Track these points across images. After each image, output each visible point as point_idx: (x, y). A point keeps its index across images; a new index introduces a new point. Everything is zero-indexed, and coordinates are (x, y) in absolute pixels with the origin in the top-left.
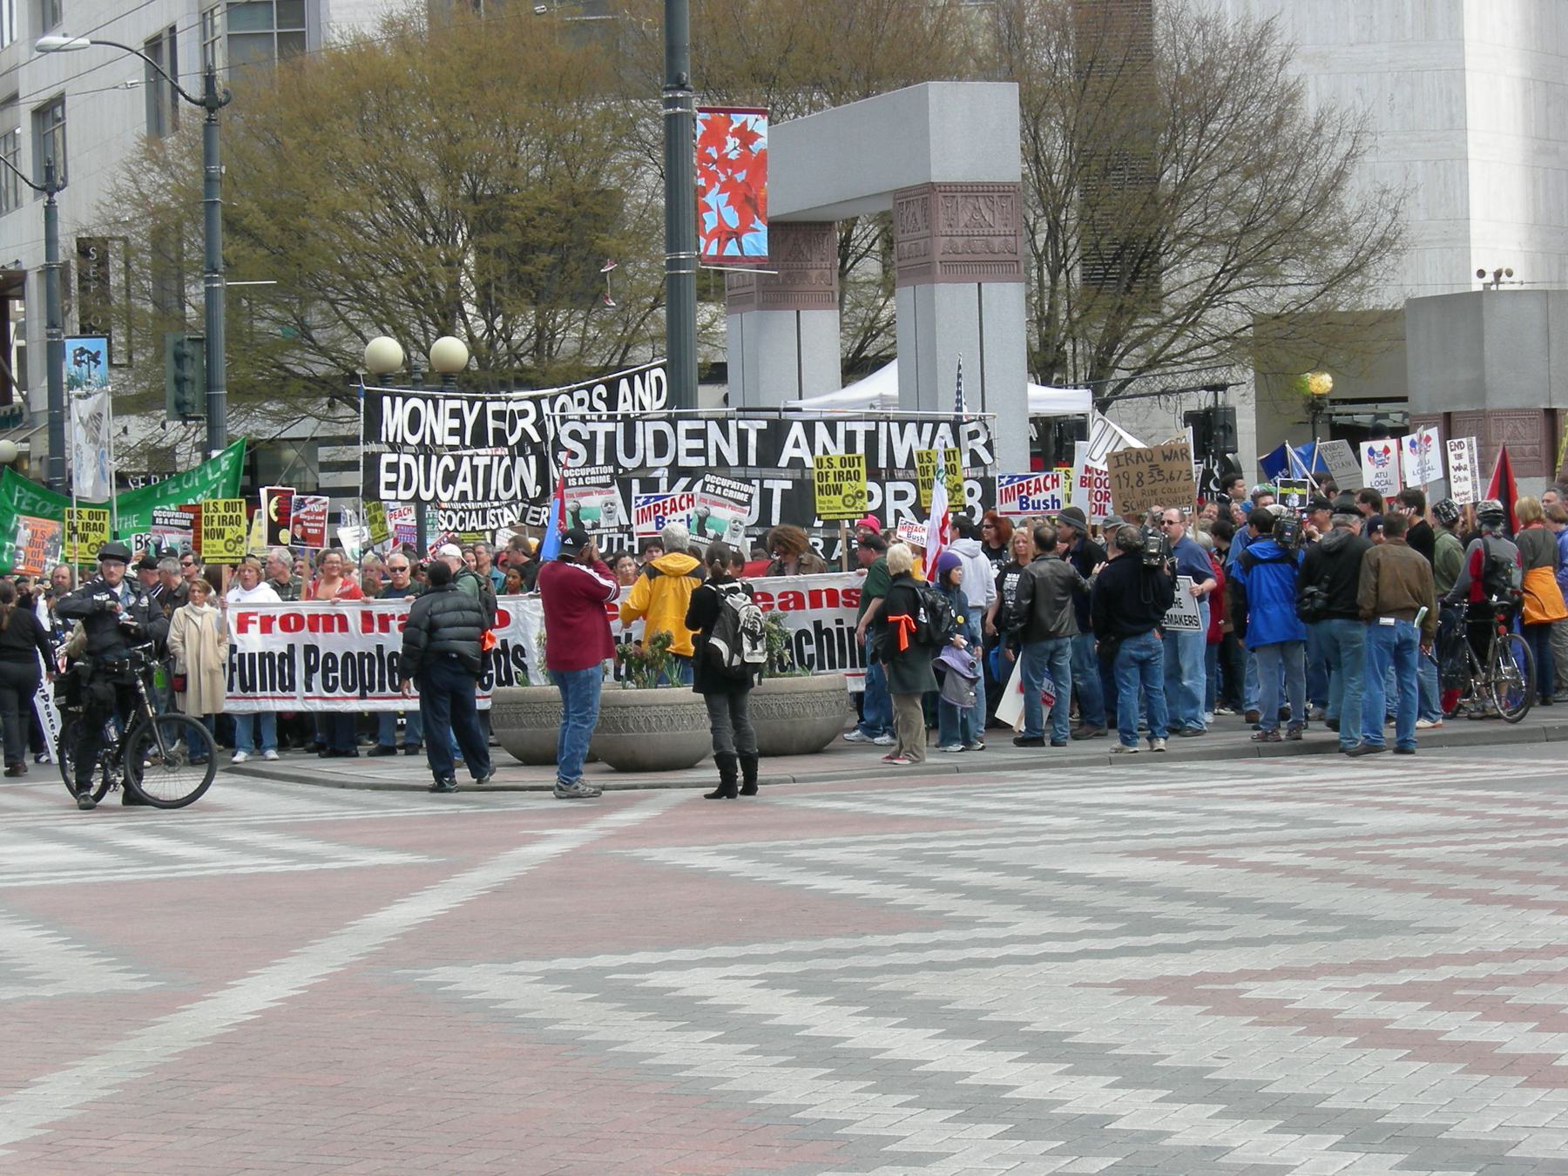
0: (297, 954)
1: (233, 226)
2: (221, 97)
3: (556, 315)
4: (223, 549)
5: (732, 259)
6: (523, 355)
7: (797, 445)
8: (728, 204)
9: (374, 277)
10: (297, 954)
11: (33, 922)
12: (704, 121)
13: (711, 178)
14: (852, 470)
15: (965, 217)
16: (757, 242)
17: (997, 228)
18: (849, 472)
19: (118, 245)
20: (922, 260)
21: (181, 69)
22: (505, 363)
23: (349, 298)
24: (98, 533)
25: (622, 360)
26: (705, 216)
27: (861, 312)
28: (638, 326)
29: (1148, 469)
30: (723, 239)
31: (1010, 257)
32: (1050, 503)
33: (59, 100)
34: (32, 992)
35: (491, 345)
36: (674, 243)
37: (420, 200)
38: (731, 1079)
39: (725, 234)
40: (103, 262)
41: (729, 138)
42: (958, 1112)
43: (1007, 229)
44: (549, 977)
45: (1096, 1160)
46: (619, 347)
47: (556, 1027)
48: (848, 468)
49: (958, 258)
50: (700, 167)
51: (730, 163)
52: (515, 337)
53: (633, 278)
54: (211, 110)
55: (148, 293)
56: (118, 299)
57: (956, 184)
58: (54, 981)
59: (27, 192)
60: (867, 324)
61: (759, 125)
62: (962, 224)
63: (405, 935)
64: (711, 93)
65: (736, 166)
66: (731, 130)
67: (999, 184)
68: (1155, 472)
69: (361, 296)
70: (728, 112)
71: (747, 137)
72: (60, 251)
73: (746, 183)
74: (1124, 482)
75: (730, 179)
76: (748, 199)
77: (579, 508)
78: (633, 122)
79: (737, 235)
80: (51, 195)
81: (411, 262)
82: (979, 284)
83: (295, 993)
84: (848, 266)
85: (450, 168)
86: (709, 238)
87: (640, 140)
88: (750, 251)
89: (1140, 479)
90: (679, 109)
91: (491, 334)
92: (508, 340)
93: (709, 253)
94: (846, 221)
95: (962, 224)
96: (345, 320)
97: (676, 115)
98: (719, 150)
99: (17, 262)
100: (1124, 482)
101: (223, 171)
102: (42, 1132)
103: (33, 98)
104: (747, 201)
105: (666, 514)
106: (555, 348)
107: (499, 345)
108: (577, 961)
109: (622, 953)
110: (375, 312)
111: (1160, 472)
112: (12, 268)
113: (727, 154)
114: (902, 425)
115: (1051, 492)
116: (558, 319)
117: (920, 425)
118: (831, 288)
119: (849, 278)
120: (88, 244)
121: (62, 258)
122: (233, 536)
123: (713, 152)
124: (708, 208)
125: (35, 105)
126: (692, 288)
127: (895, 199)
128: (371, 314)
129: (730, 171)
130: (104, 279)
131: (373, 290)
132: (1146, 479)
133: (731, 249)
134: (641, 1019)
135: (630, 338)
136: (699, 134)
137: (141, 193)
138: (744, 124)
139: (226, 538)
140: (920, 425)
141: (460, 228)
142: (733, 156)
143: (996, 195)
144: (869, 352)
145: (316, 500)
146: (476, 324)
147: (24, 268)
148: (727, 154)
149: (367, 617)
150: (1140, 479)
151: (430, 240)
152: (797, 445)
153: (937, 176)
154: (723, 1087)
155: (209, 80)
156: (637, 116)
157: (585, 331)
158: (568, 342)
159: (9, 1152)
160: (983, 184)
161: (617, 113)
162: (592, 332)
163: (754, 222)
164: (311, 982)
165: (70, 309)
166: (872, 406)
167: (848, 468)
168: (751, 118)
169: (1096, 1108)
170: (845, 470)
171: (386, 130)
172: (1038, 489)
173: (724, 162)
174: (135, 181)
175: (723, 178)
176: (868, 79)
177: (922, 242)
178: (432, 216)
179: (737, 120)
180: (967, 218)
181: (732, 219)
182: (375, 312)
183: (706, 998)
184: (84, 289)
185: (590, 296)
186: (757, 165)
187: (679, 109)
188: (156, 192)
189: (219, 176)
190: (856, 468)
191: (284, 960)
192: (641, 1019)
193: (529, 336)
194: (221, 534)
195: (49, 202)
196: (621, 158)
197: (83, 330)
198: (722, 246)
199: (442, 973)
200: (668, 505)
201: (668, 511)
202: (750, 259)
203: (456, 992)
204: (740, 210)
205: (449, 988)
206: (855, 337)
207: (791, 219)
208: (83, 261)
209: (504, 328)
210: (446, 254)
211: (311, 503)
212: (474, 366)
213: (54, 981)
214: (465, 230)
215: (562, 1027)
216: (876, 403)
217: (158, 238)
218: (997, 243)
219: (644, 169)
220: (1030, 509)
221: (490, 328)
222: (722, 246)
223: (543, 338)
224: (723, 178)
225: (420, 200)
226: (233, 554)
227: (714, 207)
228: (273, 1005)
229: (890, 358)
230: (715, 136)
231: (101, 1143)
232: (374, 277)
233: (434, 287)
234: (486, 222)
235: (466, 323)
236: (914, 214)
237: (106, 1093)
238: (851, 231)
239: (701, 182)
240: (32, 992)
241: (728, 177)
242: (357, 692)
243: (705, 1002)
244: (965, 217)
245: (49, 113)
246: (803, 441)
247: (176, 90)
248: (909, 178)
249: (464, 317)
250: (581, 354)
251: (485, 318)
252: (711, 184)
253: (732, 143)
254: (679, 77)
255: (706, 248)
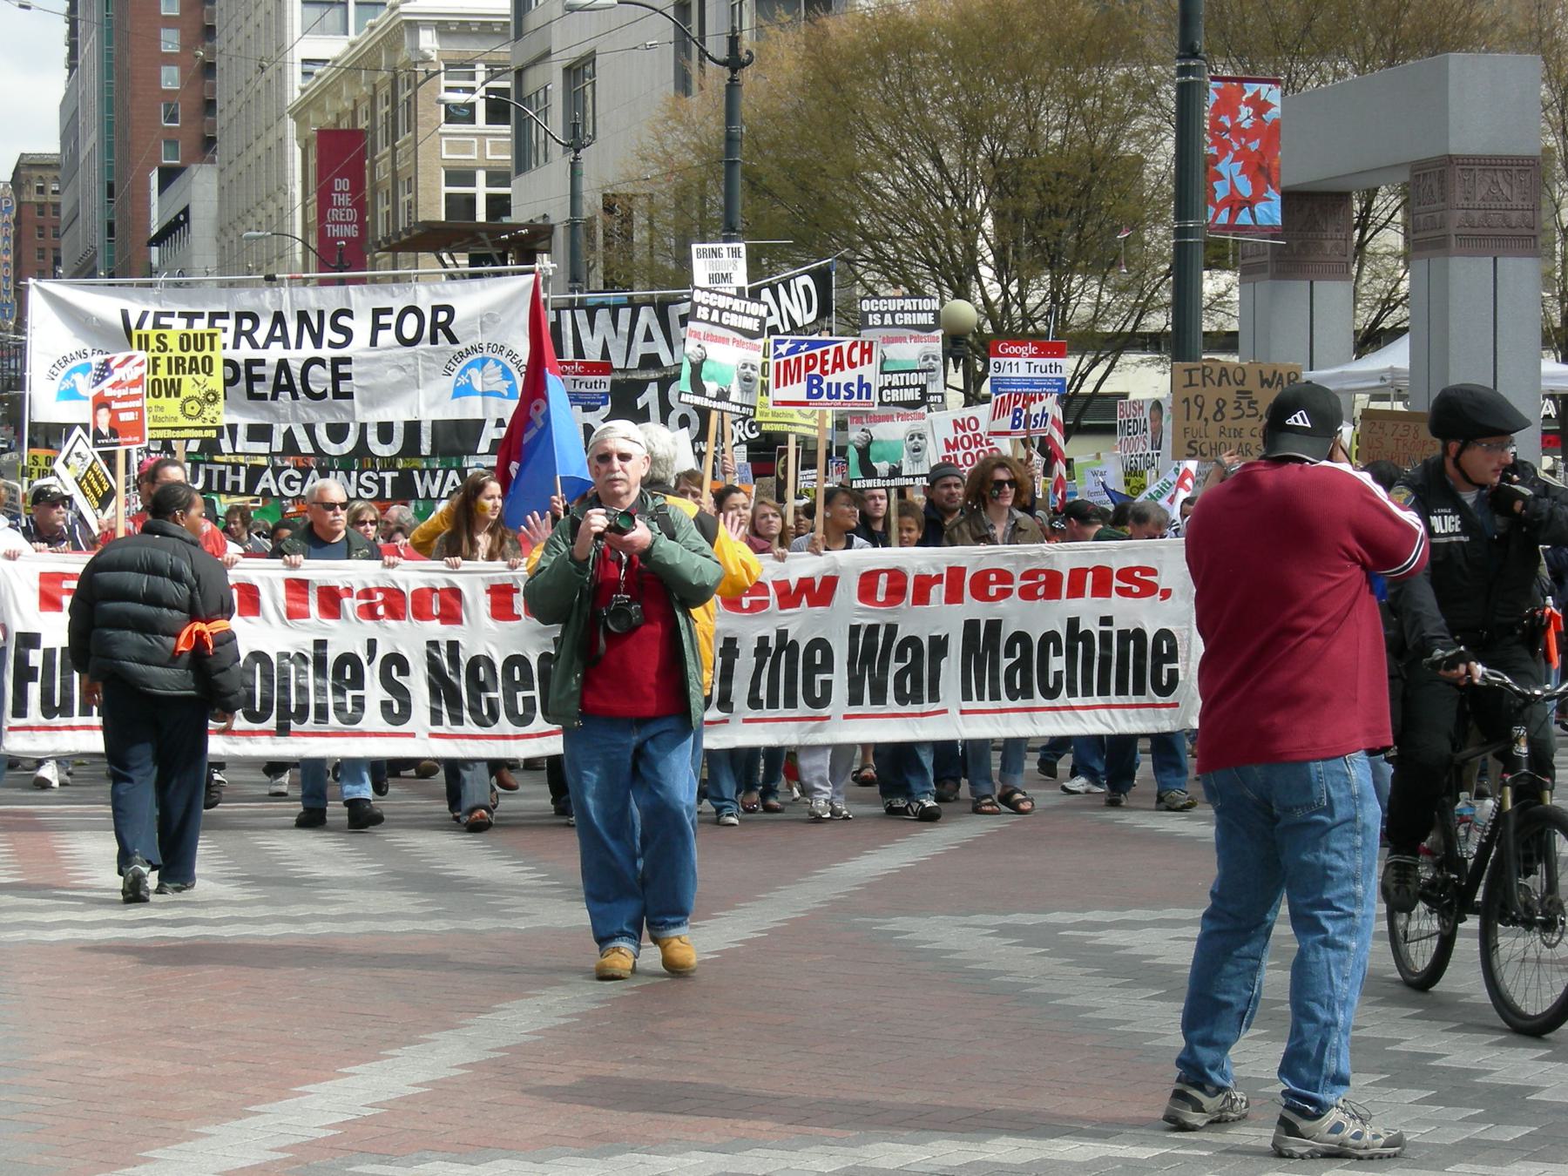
0: (761, 899)
1: (754, 183)
2: (745, 57)
3: (1070, 280)
4: (178, 413)
5: (1243, 228)
6: (1037, 319)
7: (649, 337)
8: (1242, 172)
9: (889, 237)
10: (761, 899)
11: (514, 858)
12: (1217, 90)
13: (1224, 147)
14: (200, 355)
15: (1482, 191)
16: (1270, 211)
17: (1514, 202)
18: (193, 359)
19: (642, 202)
20: (1438, 233)
21: (709, 30)
22: (1019, 327)
23: (867, 259)
24: (201, 377)
25: (1135, 327)
26: (1216, 184)
27: (1379, 284)
28: (1153, 293)
29: (1234, 397)
30: (1235, 208)
31: (1526, 231)
32: (855, 389)
33: (590, 58)
34: (504, 924)
35: (1006, 307)
36: (1181, 214)
37: (937, 161)
38: (1166, 1035)
39: (1235, 203)
40: (628, 219)
41: (1242, 107)
42: (1383, 1076)
43: (1525, 204)
44: (1004, 931)
45: (1512, 1129)
46: (1132, 314)
47: (1004, 979)
48: (192, 352)
49: (1474, 231)
50: (1212, 135)
51: (1244, 132)
52: (1028, 301)
53: (1149, 244)
54: (734, 71)
55: (668, 249)
56: (640, 255)
57: (1474, 157)
58: (528, 915)
59: (556, 150)
60: (1385, 296)
61: (1272, 94)
62: (1478, 198)
63: (868, 885)
64: (1234, 60)
65: (1249, 135)
66: (1244, 98)
67: (1518, 158)
68: (1245, 403)
69: (879, 259)
70: (1241, 80)
71: (1260, 106)
72: (585, 207)
73: (1261, 153)
74: (1195, 410)
75: (1244, 147)
76: (1260, 168)
77: (870, 441)
78: (1153, 89)
79: (1250, 203)
80: (577, 151)
81: (929, 225)
82: (1495, 259)
83: (755, 935)
84: (1367, 236)
85: (972, 129)
86: (1219, 208)
87: (1161, 106)
88: (1263, 220)
89: (1220, 410)
90: (1191, 78)
91: (1006, 298)
92: (1022, 305)
93: (1218, 222)
94: (1368, 191)
95: (1478, 198)
96: (863, 281)
97: (1189, 83)
98: (1233, 119)
99: (545, 216)
100: (1195, 410)
101: (744, 131)
102: (498, 1054)
103: (565, 54)
104: (1260, 170)
105: (825, 373)
106: (1069, 313)
107: (1013, 310)
108: (1033, 916)
109: (1078, 911)
110: (892, 273)
111: (1252, 403)
112: (540, 222)
113: (1240, 123)
114: (591, 312)
115: (859, 370)
116: (1073, 285)
117: (615, 311)
118: (1346, 259)
119: (1369, 248)
120: (613, 200)
121: (586, 214)
122: (198, 392)
123: (1226, 120)
124: (1220, 177)
125: (566, 63)
126: (1200, 256)
127: (1412, 171)
128: (887, 275)
129: (1243, 140)
130: (628, 237)
131: (890, 251)
132: (1229, 410)
133: (1244, 218)
134: (1087, 975)
135: (1145, 305)
136: (1211, 103)
137: (665, 152)
138: (1258, 93)
139: (185, 393)
140: (615, 311)
141: (978, 192)
142: (1246, 125)
143: (1514, 168)
144: (1387, 324)
145: (129, 359)
146: (991, 287)
147: (551, 222)
148: (1240, 123)
149: (297, 587)
150: (1220, 410)
151: (949, 202)
152: (649, 337)
153: (1456, 147)
154: (1157, 1042)
155: (734, 41)
156: (1159, 83)
157: (1099, 296)
158: (1081, 310)
159: (464, 1071)
160: (1501, 157)
161: (1139, 80)
162: (1106, 298)
163: (1267, 191)
164: (772, 926)
165: (594, 265)
166: (1382, 379)
167: (192, 352)
168: (1264, 88)
169: (1522, 1079)
170: (187, 356)
171: (907, 93)
172: (838, 365)
173: (1237, 131)
174: (659, 139)
175: (1236, 147)
176: (1394, 47)
177: (1438, 215)
178: (951, 179)
179: (1250, 90)
180: (1484, 192)
181: (1245, 188)
182: (892, 273)
183: (1154, 957)
184: (607, 245)
185: (1102, 265)
186: (1270, 135)
187: (1191, 78)
188: (679, 150)
189: (739, 136)
190: (207, 352)
191: (748, 904)
192: (1087, 975)
193: (1043, 301)
194: (173, 389)
195: (575, 159)
196: (1140, 123)
197: (606, 285)
198: (1234, 214)
199: (898, 923)
200: (829, 357)
201: (828, 367)
202: (1263, 228)
203: (910, 941)
204: (1252, 179)
205: (905, 937)
206: (1373, 308)
207: (1306, 189)
208: (607, 218)
209: (1020, 293)
210: (963, 218)
211: (120, 365)
212: (988, 328)
213: (528, 915)
214: (982, 192)
215: (1009, 979)
216: (1387, 376)
217: (682, 196)
218: (1514, 217)
219: (1164, 135)
220: (824, 398)
221: (1005, 292)
222: (1234, 214)
223: (1059, 299)
224: (1236, 147)
225: (937, 161)
226: (198, 423)
227: (1226, 174)
228: (734, 946)
229: (1406, 330)
230: (1228, 105)
231: (551, 1067)
232: (889, 237)
233: (951, 251)
234: (1004, 181)
235: (982, 288)
236: (1430, 186)
237: (563, 1021)
238: (1371, 202)
239: (1213, 151)
240: (504, 924)
241: (1241, 145)
242: (272, 722)
243: (1151, 961)
244: (1482, 191)
245: (579, 72)
246: (658, 334)
247: (703, 53)
248: (1426, 150)
249: (979, 280)
250: (1095, 320)
251: (1000, 281)
252: (1224, 153)
253: (1245, 112)
254: (1193, 46)
255: (1215, 217)
